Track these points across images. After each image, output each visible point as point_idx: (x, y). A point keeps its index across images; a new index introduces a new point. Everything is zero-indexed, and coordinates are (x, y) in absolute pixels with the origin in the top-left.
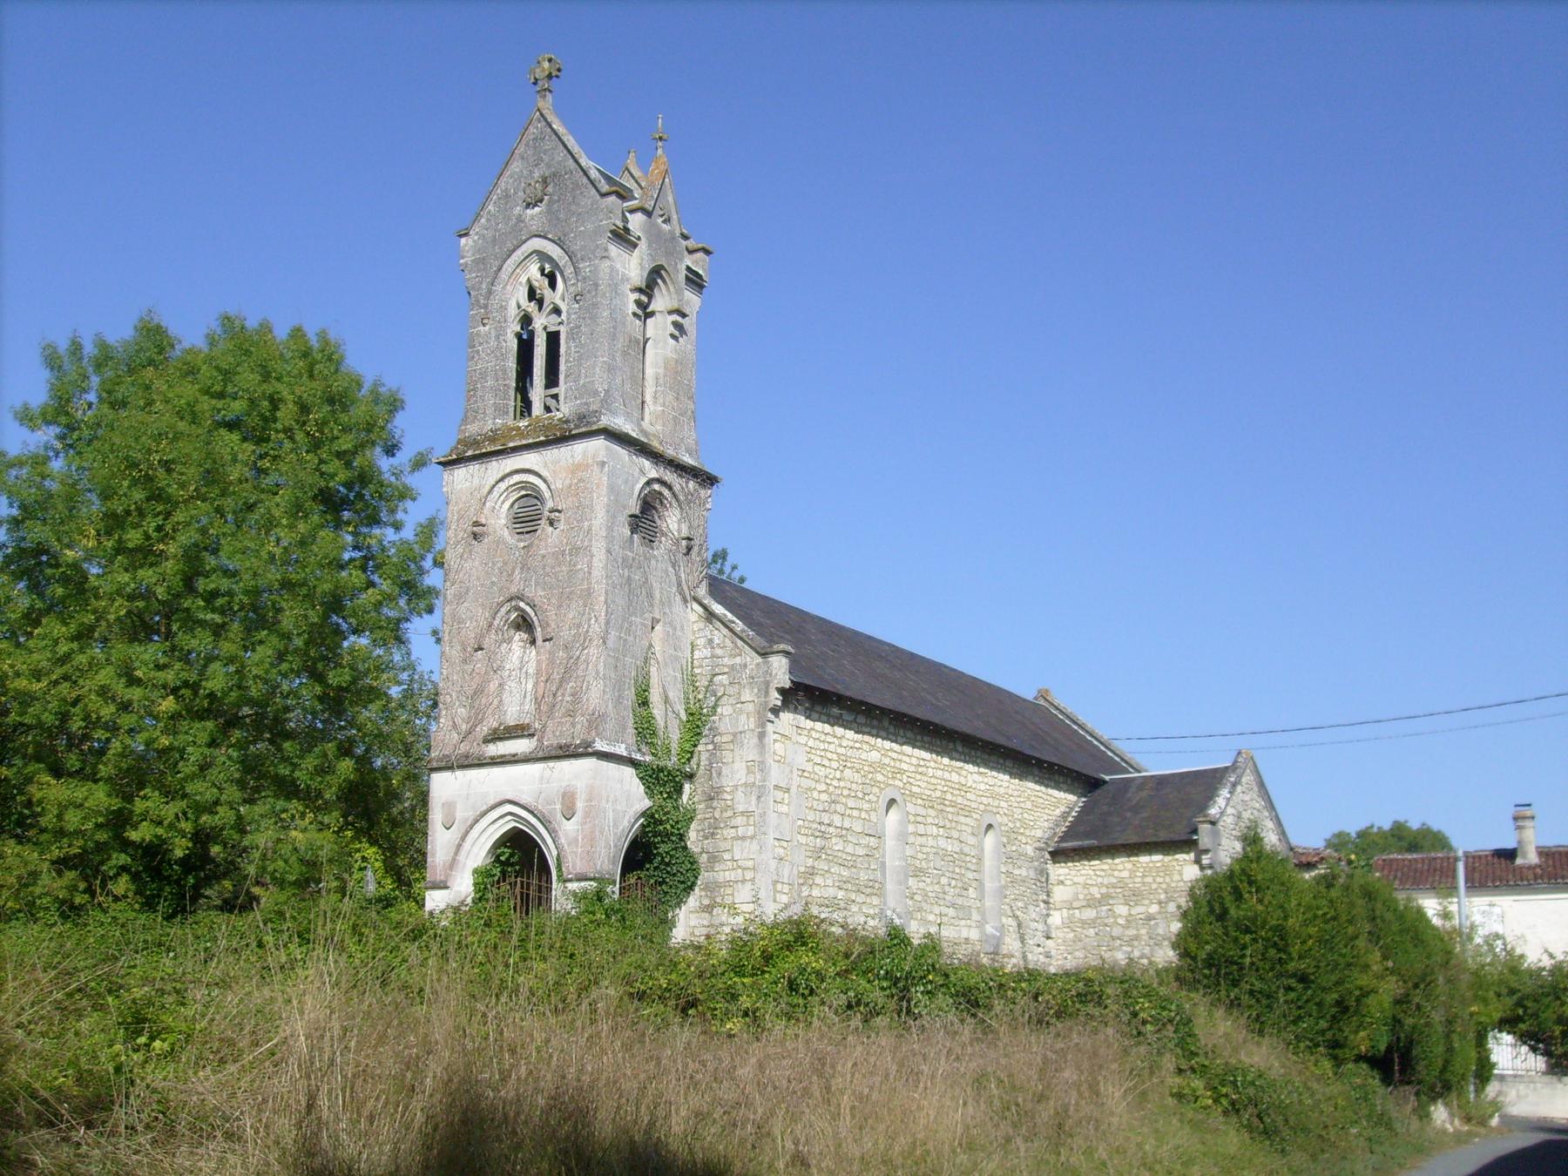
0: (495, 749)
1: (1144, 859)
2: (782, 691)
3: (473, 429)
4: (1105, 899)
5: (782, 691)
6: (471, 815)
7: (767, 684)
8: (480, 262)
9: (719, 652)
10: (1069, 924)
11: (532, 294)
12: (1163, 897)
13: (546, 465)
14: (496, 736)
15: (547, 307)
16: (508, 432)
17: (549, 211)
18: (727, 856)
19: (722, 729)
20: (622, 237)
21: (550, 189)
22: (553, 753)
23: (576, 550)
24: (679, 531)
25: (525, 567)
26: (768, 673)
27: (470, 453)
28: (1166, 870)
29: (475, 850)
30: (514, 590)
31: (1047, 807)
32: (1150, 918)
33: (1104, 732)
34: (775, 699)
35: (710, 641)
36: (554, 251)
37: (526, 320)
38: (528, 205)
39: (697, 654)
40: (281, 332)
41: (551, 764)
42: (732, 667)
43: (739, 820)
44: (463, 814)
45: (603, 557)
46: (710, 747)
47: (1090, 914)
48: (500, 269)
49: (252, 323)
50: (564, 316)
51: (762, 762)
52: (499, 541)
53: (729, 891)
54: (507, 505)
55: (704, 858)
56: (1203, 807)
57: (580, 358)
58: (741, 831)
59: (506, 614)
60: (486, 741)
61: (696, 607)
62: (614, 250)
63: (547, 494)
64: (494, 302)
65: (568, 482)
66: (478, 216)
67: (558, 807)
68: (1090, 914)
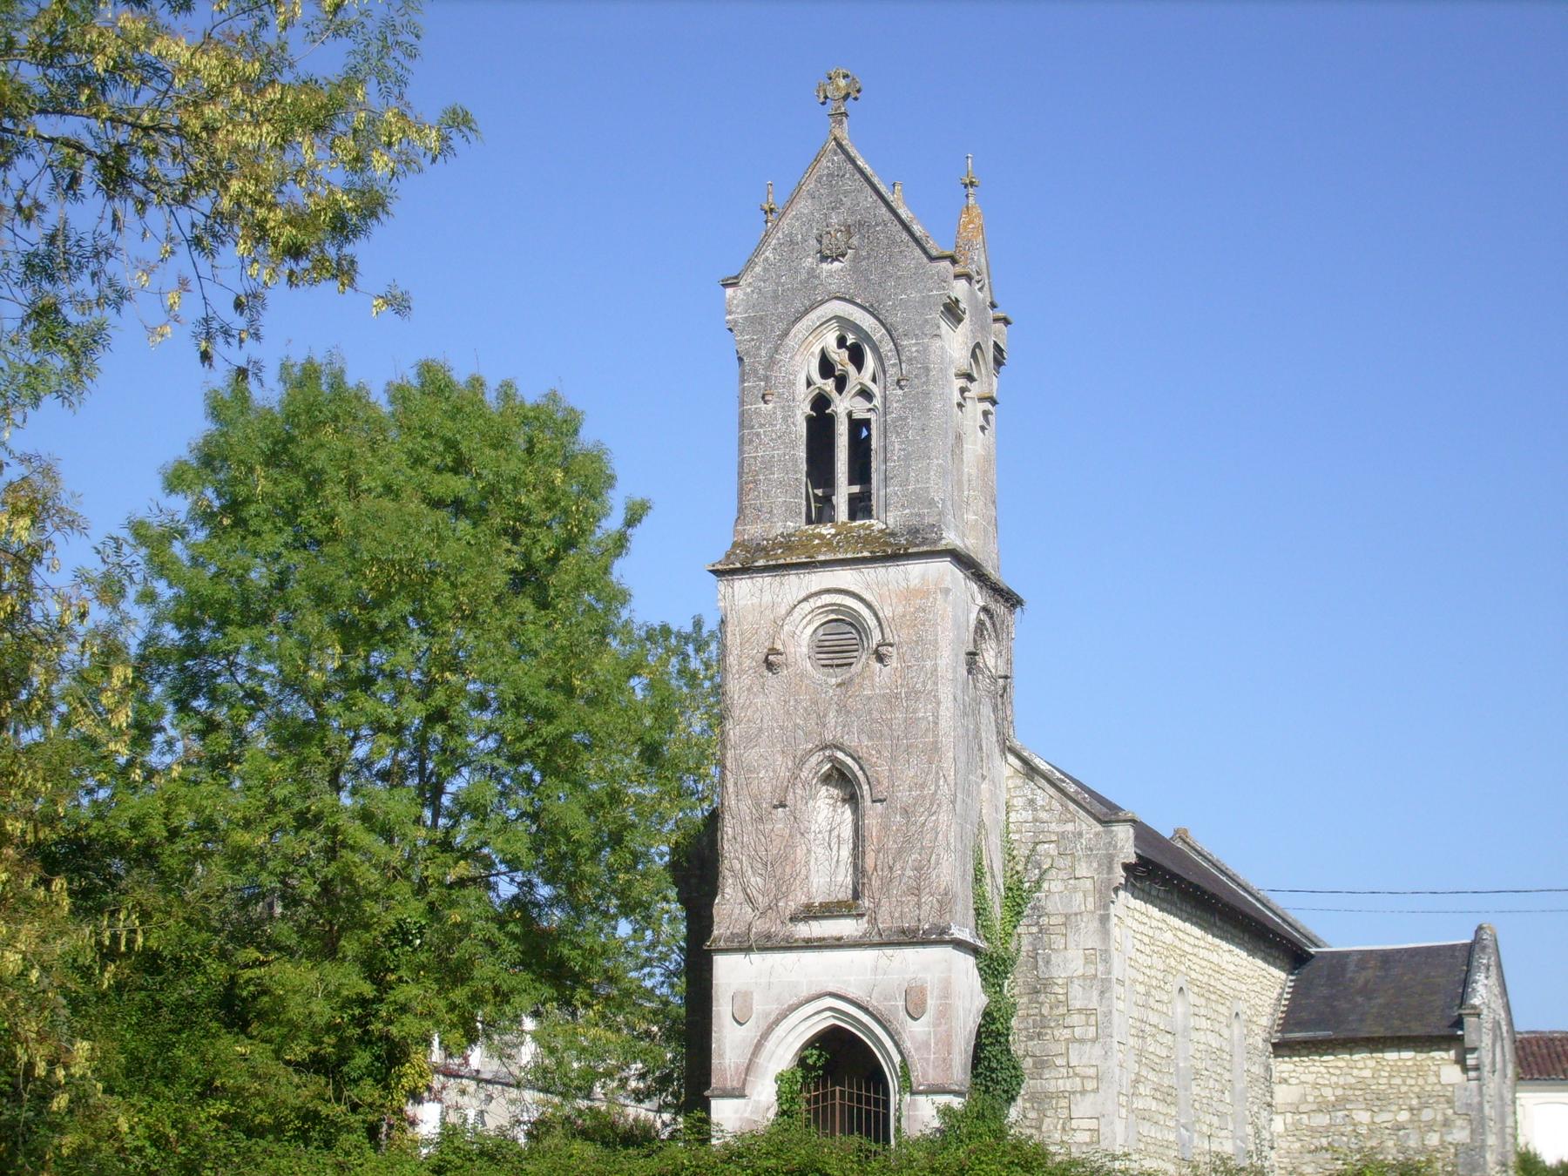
0: (804, 930)
1: (1391, 1056)
2: (1126, 867)
3: (754, 531)
4: (1340, 1103)
5: (1126, 867)
6: (774, 1009)
7: (1111, 859)
8: (757, 322)
9: (1043, 815)
10: (1293, 1132)
11: (826, 367)
12: (1415, 1102)
14: (810, 913)
15: (852, 386)
16: (805, 543)
17: (855, 268)
18: (1059, 1061)
19: (1050, 908)
20: (952, 311)
21: (855, 241)
22: (894, 938)
23: (914, 694)
24: (996, 667)
25: (843, 709)
26: (1111, 844)
27: (761, 563)
28: (1420, 1071)
29: (780, 1051)
30: (829, 737)
31: (1261, 985)
32: (1399, 1127)
33: (1254, 883)
34: (1120, 876)
35: (1032, 802)
36: (866, 321)
38: (824, 258)
39: (1013, 817)
41: (889, 951)
42: (1062, 835)
43: (1076, 1019)
44: (762, 1007)
45: (950, 705)
46: (1034, 930)
47: (1322, 1120)
48: (786, 334)
49: (460, 376)
52: (803, 675)
53: (1064, 1103)
55: (1028, 1063)
56: (1463, 999)
57: (907, 457)
58: (1078, 1032)
59: (817, 763)
61: (1011, 759)
64: (778, 374)
65: (900, 610)
66: (750, 263)
68: (1322, 1120)
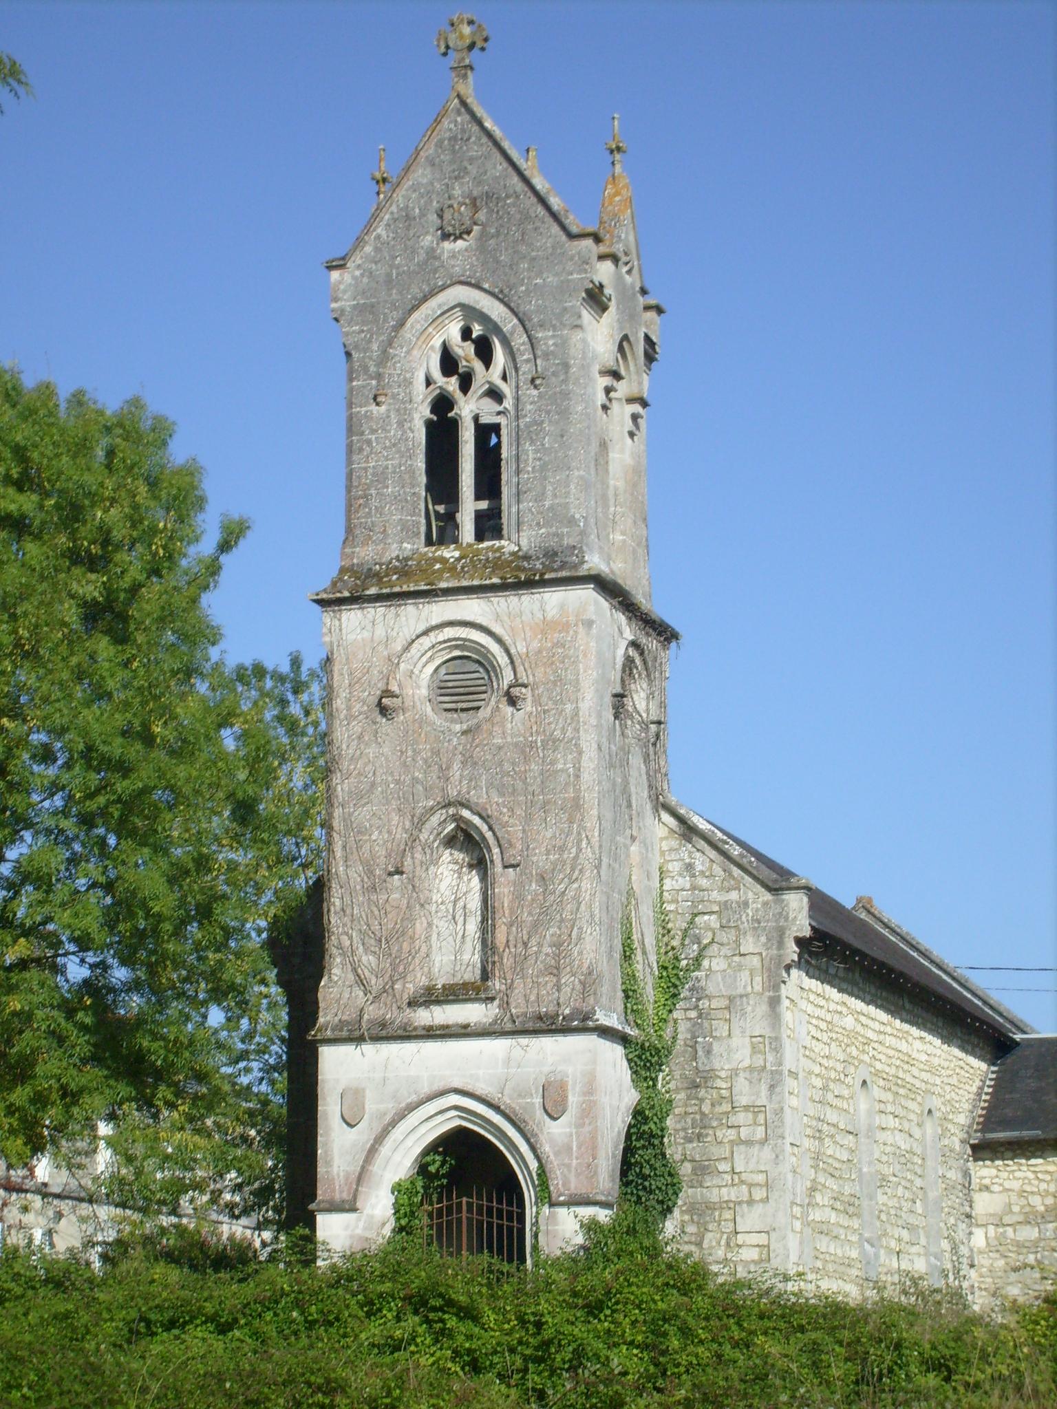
2: (800, 942)
3: (365, 554)
5: (800, 942)
6: (390, 1108)
7: (781, 932)
8: (367, 311)
9: (704, 882)
10: (997, 1246)
11: (449, 363)
13: (498, 617)
14: (430, 997)
15: (479, 386)
16: (424, 568)
17: (481, 247)
19: (711, 989)
21: (482, 216)
22: (530, 1026)
23: (552, 742)
25: (468, 760)
26: (782, 915)
27: (373, 591)
33: (950, 961)
35: (689, 867)
36: (495, 310)
37: (442, 404)
38: (446, 236)
39: (668, 884)
40: (64, 392)
41: (524, 1041)
42: (725, 905)
43: (741, 1118)
44: (376, 1106)
46: (693, 1014)
48: (401, 324)
50: (508, 403)
51: (777, 1039)
52: (422, 721)
53: (728, 1215)
54: (430, 669)
55: (686, 1169)
57: (543, 468)
58: (744, 1133)
59: (439, 824)
60: (413, 1003)
61: (666, 817)
62: (587, 316)
63: (502, 659)
64: (393, 372)
65: (535, 645)
66: (359, 242)
67: (538, 1100)
